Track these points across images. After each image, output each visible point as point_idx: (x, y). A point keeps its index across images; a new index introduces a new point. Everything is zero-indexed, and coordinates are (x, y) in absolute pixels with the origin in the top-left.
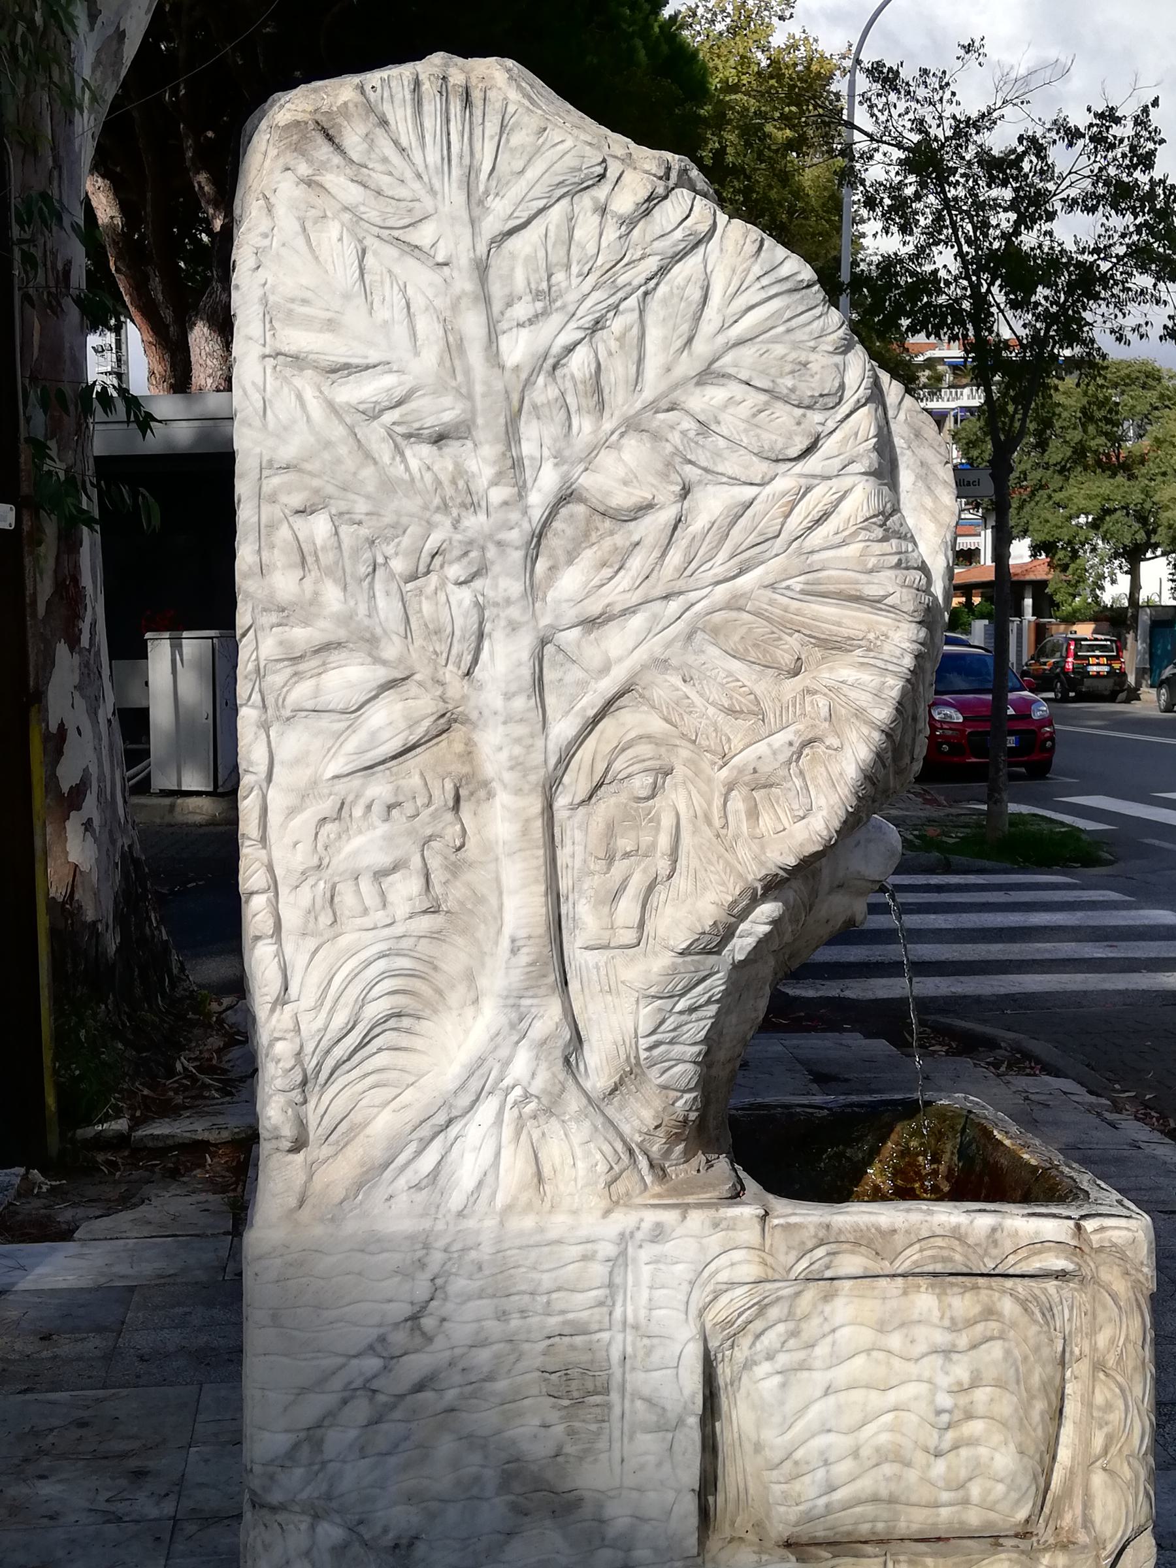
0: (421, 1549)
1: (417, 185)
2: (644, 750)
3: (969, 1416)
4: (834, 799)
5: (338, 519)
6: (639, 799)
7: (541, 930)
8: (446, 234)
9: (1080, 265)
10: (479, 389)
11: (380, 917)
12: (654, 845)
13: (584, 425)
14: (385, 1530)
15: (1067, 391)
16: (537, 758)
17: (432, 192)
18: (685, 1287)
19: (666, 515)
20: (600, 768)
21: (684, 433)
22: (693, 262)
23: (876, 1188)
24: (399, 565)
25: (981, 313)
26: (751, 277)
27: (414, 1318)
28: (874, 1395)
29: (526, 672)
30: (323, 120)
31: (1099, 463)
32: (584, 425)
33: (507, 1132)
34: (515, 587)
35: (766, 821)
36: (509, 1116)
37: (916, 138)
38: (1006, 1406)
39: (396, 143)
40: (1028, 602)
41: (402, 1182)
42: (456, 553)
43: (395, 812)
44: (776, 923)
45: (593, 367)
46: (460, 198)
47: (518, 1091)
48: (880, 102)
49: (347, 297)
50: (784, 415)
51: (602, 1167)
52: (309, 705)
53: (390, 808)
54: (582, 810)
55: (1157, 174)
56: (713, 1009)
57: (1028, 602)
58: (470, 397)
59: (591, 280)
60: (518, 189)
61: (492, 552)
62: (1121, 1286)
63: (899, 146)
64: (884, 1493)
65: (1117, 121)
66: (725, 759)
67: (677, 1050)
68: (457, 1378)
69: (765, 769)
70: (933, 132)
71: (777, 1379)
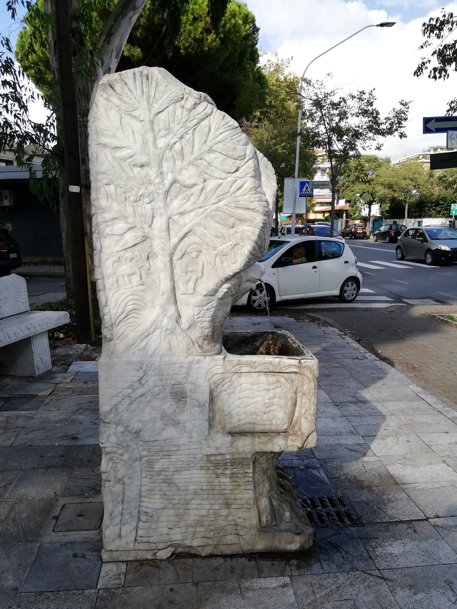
0: (142, 433)
1: (135, 100)
2: (195, 246)
3: (273, 405)
4: (242, 259)
5: (116, 186)
6: (194, 258)
7: (169, 289)
8: (142, 113)
9: (355, 130)
10: (151, 153)
11: (129, 286)
12: (197, 270)
13: (178, 163)
14: (133, 429)
15: (353, 163)
16: (168, 247)
17: (139, 102)
18: (205, 374)
19: (200, 187)
20: (184, 250)
21: (204, 166)
22: (205, 122)
23: (261, 352)
24: (132, 198)
25: (330, 143)
26: (221, 125)
27: (140, 380)
28: (250, 399)
29: (165, 226)
30: (110, 83)
31: (362, 180)
32: (178, 163)
33: (163, 337)
34: (161, 204)
35: (225, 264)
36: (163, 334)
37: (315, 98)
38: (282, 402)
39: (129, 89)
40: (344, 215)
41: (137, 349)
42: (147, 195)
43: (133, 260)
44: (229, 289)
45: (181, 148)
46: (146, 104)
47: (165, 328)
48: (306, 88)
49: (117, 129)
50: (230, 161)
51: (186, 346)
52: (110, 233)
53: (131, 259)
54: (180, 261)
55: (374, 107)
56: (213, 309)
57: (344, 215)
58: (149, 155)
59: (180, 125)
60: (161, 101)
61: (155, 195)
62: (310, 376)
63: (311, 99)
64: (252, 422)
65: (364, 94)
66: (215, 249)
67: (204, 319)
68: (150, 394)
69: (225, 251)
70: (319, 96)
71: (227, 395)
